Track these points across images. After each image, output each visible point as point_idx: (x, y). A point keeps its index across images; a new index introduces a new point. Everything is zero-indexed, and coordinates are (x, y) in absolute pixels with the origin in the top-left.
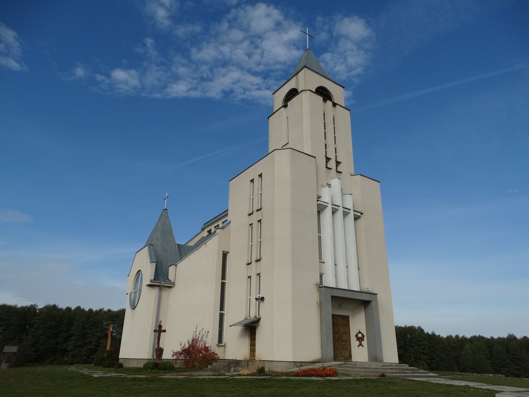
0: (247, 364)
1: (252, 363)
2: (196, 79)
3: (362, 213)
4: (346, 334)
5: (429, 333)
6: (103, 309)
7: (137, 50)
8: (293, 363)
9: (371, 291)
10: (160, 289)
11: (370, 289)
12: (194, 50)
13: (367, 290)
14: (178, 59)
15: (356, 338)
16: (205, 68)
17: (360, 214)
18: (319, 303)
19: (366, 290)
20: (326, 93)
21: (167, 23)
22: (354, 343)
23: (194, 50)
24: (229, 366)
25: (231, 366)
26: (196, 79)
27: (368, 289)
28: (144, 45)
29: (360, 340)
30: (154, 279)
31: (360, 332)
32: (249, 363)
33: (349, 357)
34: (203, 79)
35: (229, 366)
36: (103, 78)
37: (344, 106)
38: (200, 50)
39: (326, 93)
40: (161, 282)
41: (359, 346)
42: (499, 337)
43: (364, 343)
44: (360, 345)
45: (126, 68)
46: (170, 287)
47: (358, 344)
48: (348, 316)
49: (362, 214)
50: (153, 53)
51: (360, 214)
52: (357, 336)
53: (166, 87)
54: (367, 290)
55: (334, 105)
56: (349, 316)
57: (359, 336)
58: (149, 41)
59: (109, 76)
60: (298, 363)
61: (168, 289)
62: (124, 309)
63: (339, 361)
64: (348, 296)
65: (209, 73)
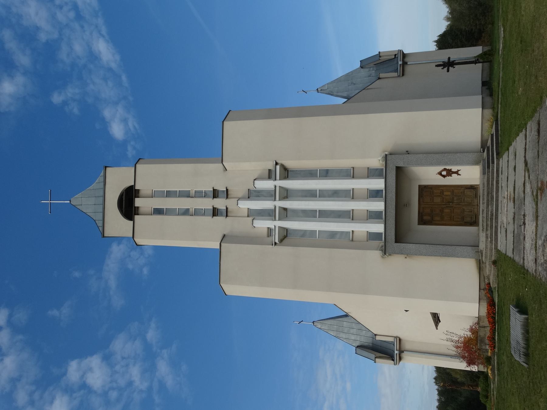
0: (482, 328)
1: (481, 321)
2: (82, 27)
3: (275, 163)
4: (442, 192)
5: (436, 39)
6: (444, 20)
7: (76, 111)
8: (480, 301)
9: (382, 156)
10: (403, 352)
11: (380, 158)
12: (43, 37)
13: (381, 161)
14: (63, 55)
15: (447, 177)
16: (60, 16)
17: (278, 167)
18: (406, 256)
19: (381, 162)
20: (124, 197)
21: (20, 79)
22: (453, 180)
23: (43, 37)
24: (484, 351)
25: (484, 349)
26: (82, 27)
27: (380, 160)
28: (65, 103)
29: (450, 173)
30: (393, 360)
31: (440, 174)
32: (481, 326)
33: (472, 188)
34: (79, 17)
35: (484, 351)
36: (130, 148)
37: (133, 169)
38: (38, 28)
39: (124, 197)
40: (395, 354)
41: (458, 174)
42: (436, 41)
43: (454, 169)
44: (457, 173)
45: (105, 124)
46: (400, 340)
47: (457, 175)
48: (420, 186)
49: (277, 164)
50: (71, 91)
51: (278, 167)
52: (444, 176)
53: (110, 70)
54: (381, 161)
55: (137, 191)
56: (419, 185)
57: (445, 174)
58: (57, 98)
59: (124, 144)
60: (480, 295)
61: (402, 342)
62: (436, 45)
63: (478, 208)
64: (393, 222)
65: (65, 9)
